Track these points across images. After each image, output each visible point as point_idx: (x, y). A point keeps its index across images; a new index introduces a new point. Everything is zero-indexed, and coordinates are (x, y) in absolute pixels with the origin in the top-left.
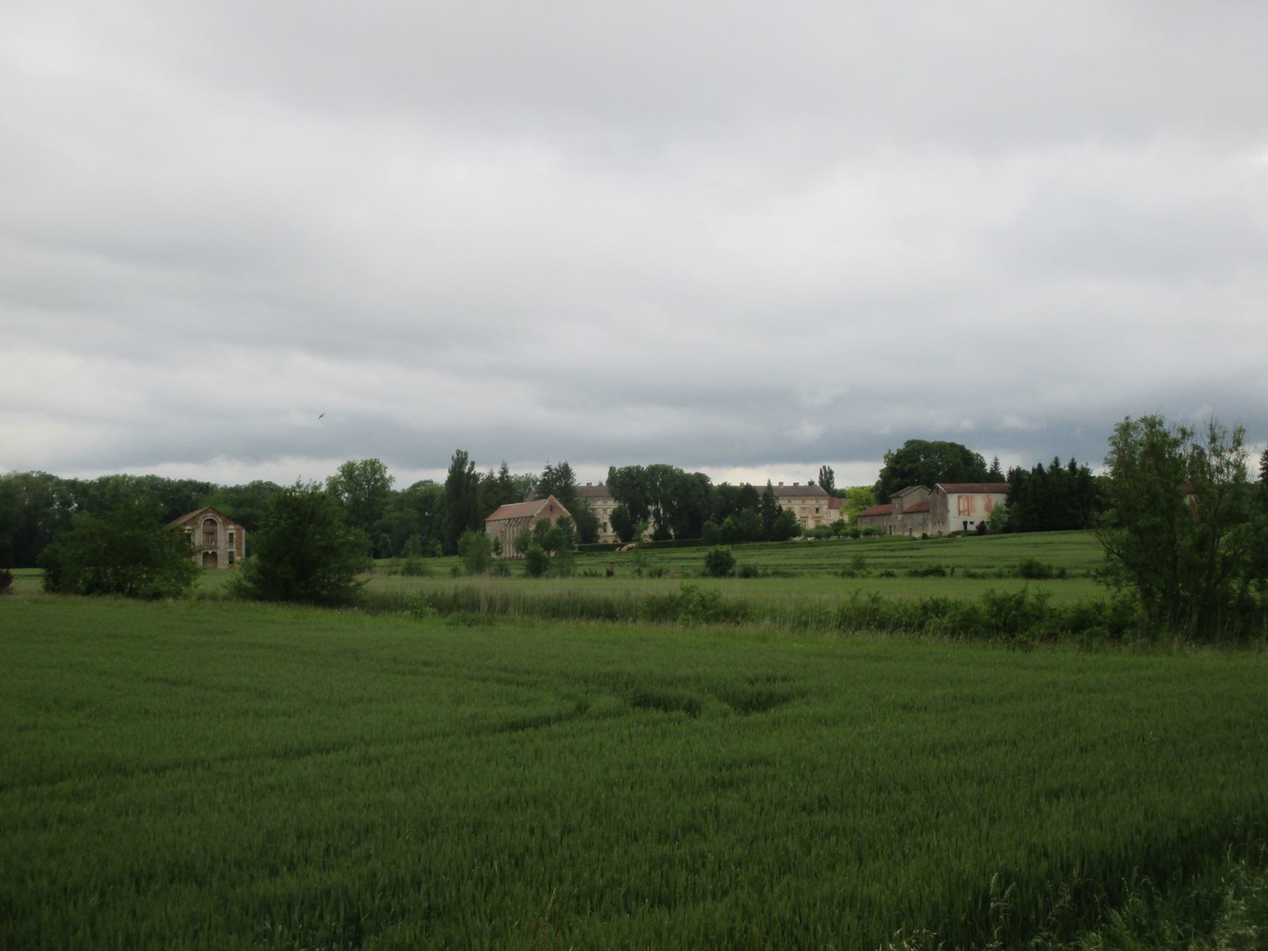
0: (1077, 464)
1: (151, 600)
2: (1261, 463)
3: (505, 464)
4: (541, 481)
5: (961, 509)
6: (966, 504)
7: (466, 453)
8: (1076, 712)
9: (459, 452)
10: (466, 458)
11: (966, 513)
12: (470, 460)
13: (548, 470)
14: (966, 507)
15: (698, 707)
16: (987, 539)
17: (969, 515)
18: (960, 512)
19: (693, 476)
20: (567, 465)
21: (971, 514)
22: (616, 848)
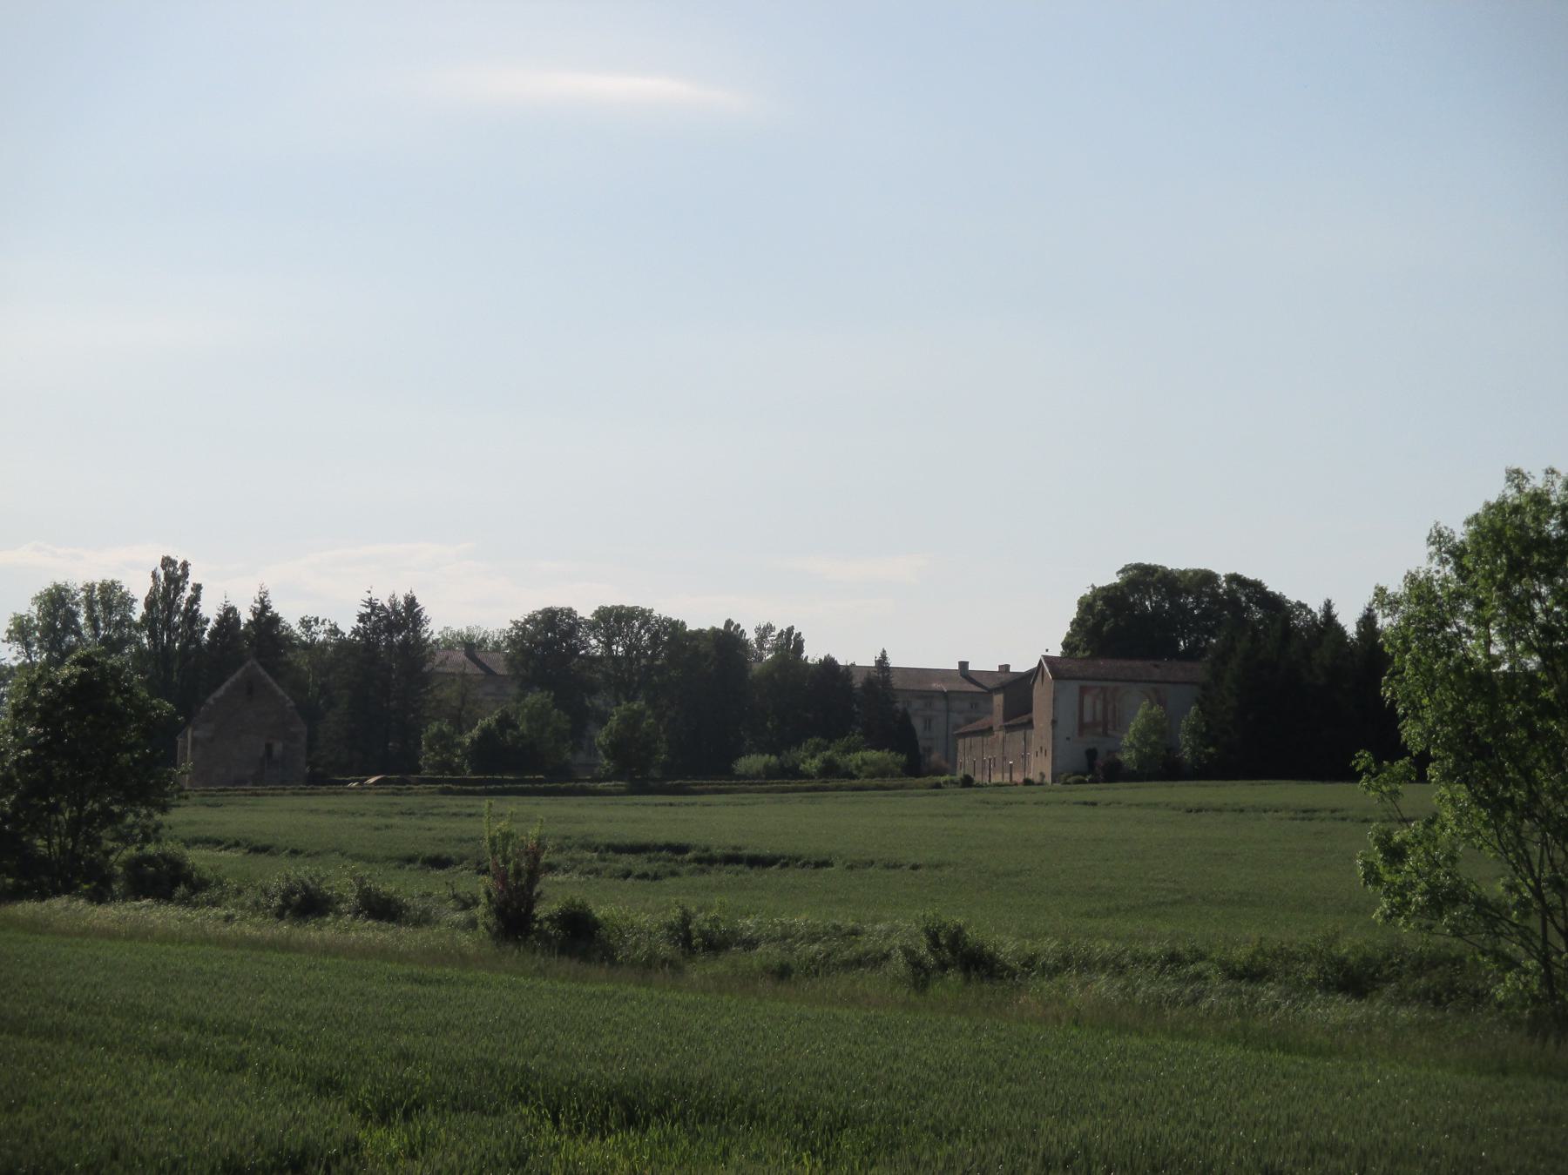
0: (430, 627)
1: (260, 853)
2: (764, 632)
3: (266, 593)
4: (1550, 594)
5: (1088, 718)
6: (1099, 707)
7: (185, 565)
8: (889, 1100)
9: (167, 562)
10: (186, 575)
11: (1100, 730)
12: (192, 579)
13: (369, 610)
14: (1099, 717)
15: (1205, 956)
16: (1097, 789)
17: (1105, 733)
18: (1082, 727)
19: (344, 646)
20: (413, 599)
21: (1110, 732)
22: (702, 1139)
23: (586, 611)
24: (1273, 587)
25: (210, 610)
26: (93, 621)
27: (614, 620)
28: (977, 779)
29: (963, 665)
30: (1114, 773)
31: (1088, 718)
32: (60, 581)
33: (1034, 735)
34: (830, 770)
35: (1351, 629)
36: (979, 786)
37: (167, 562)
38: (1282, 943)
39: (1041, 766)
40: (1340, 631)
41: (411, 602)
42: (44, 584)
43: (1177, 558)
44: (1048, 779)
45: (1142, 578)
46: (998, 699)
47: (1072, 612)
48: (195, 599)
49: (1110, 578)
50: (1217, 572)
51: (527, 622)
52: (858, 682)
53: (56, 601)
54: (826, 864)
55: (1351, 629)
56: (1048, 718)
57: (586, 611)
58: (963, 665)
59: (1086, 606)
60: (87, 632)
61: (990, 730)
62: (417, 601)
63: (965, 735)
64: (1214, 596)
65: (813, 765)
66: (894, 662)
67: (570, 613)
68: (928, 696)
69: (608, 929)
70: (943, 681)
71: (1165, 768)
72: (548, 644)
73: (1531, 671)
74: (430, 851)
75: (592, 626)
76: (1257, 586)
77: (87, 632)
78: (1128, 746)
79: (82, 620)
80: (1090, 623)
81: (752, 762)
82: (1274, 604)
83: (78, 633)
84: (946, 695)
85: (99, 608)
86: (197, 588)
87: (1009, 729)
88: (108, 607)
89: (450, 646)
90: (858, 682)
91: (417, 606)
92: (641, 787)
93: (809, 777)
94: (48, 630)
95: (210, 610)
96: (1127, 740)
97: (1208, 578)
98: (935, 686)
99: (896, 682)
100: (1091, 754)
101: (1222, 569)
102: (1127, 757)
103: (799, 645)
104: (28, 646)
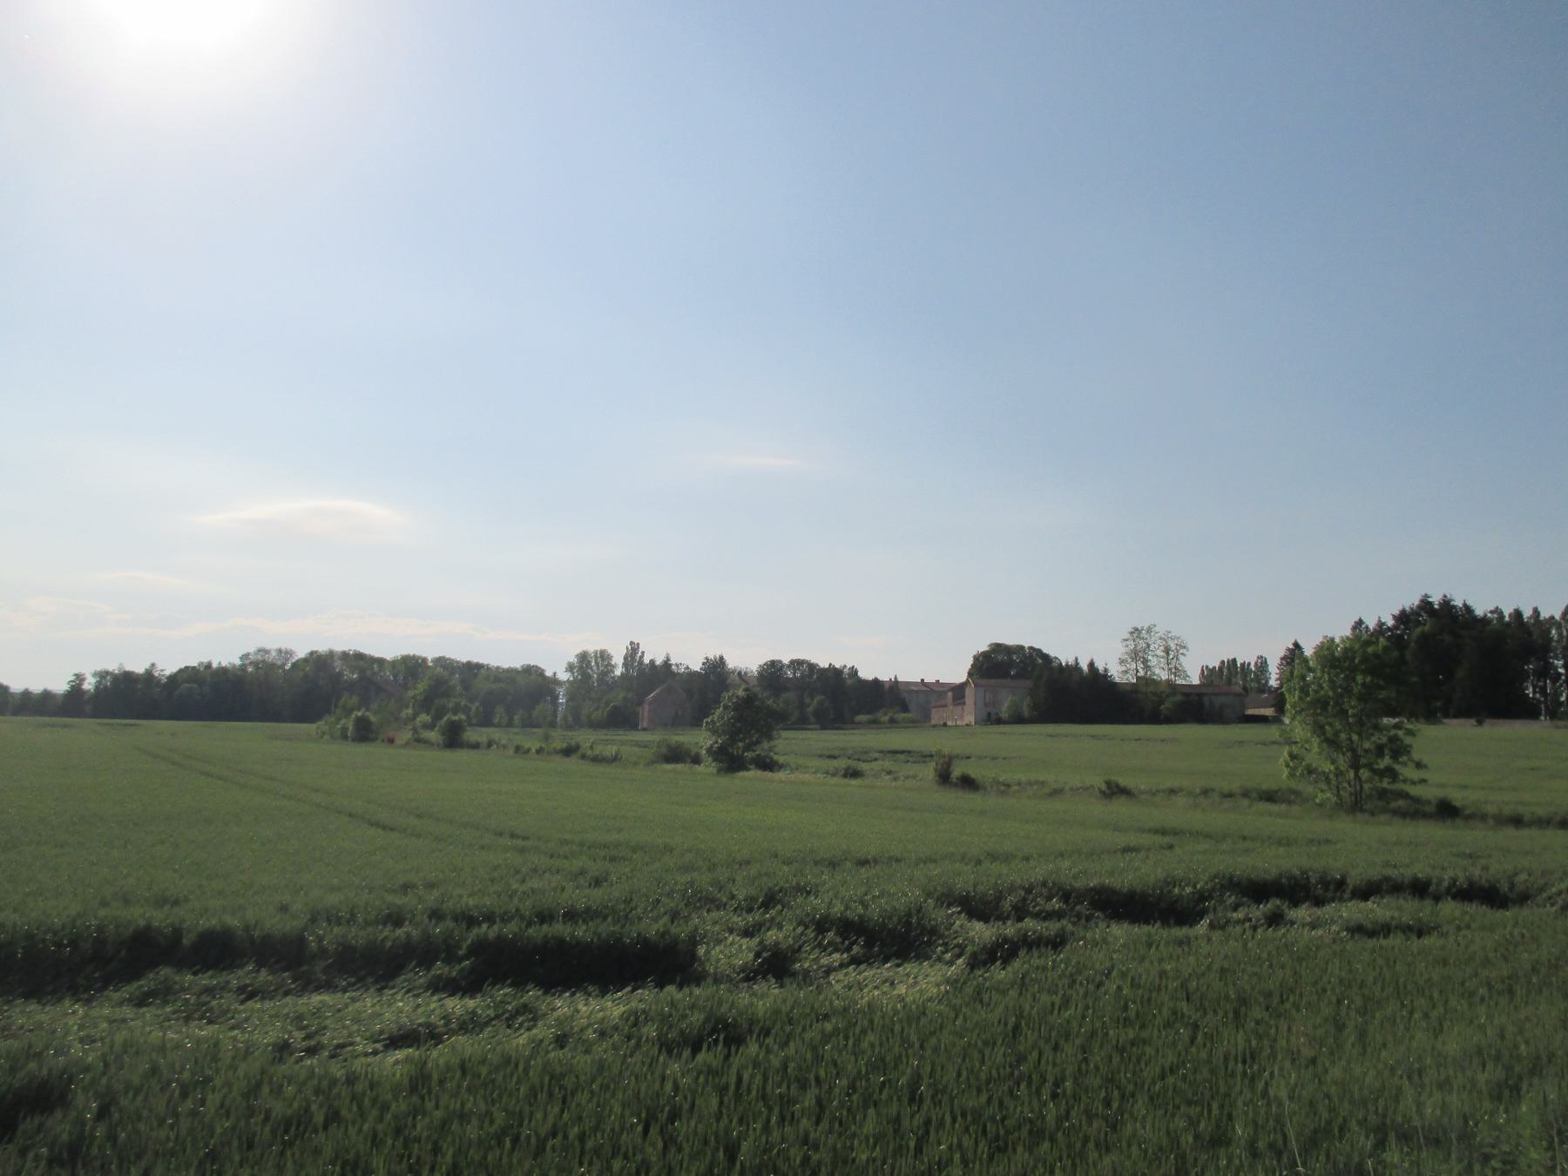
5: (987, 700)
7: (638, 644)
9: (632, 643)
10: (638, 648)
12: (641, 650)
18: (986, 705)
23: (786, 661)
24: (1045, 651)
25: (646, 661)
26: (597, 663)
27: (796, 664)
28: (949, 723)
29: (922, 680)
30: (999, 721)
31: (987, 700)
32: (585, 649)
33: (966, 708)
34: (892, 721)
35: (1085, 667)
36: (949, 726)
37: (632, 643)
38: (340, 911)
39: (970, 718)
40: (1080, 670)
41: (721, 658)
42: (579, 651)
43: (1010, 641)
44: (973, 723)
45: (998, 648)
46: (950, 694)
47: (971, 661)
48: (642, 657)
49: (984, 648)
50: (1246, 656)
51: (764, 665)
52: (887, 686)
53: (583, 657)
54: (968, 758)
55: (1085, 667)
56: (972, 700)
57: (786, 661)
58: (922, 680)
59: (976, 658)
60: (595, 668)
61: (946, 706)
62: (1096, 665)
63: (935, 707)
64: (1024, 655)
65: (886, 718)
66: (900, 679)
67: (780, 662)
68: (910, 692)
69: (1298, 740)
70: (916, 686)
71: (1018, 719)
72: (772, 674)
73: (97, 688)
74: (829, 753)
75: (789, 666)
76: (1039, 651)
77: (595, 668)
78: (1004, 710)
79: (593, 664)
80: (978, 665)
81: (860, 718)
82: (1046, 657)
83: (591, 668)
84: (916, 692)
85: (599, 659)
86: (643, 653)
87: (955, 705)
88: (603, 659)
89: (733, 672)
90: (887, 686)
91: (1262, 665)
92: (824, 728)
93: (884, 723)
94: (581, 668)
95: (646, 661)
96: (1004, 709)
97: (1022, 648)
98: (913, 688)
99: (902, 688)
100: (989, 714)
101: (1026, 645)
102: (1004, 715)
103: (856, 672)
104: (573, 673)
